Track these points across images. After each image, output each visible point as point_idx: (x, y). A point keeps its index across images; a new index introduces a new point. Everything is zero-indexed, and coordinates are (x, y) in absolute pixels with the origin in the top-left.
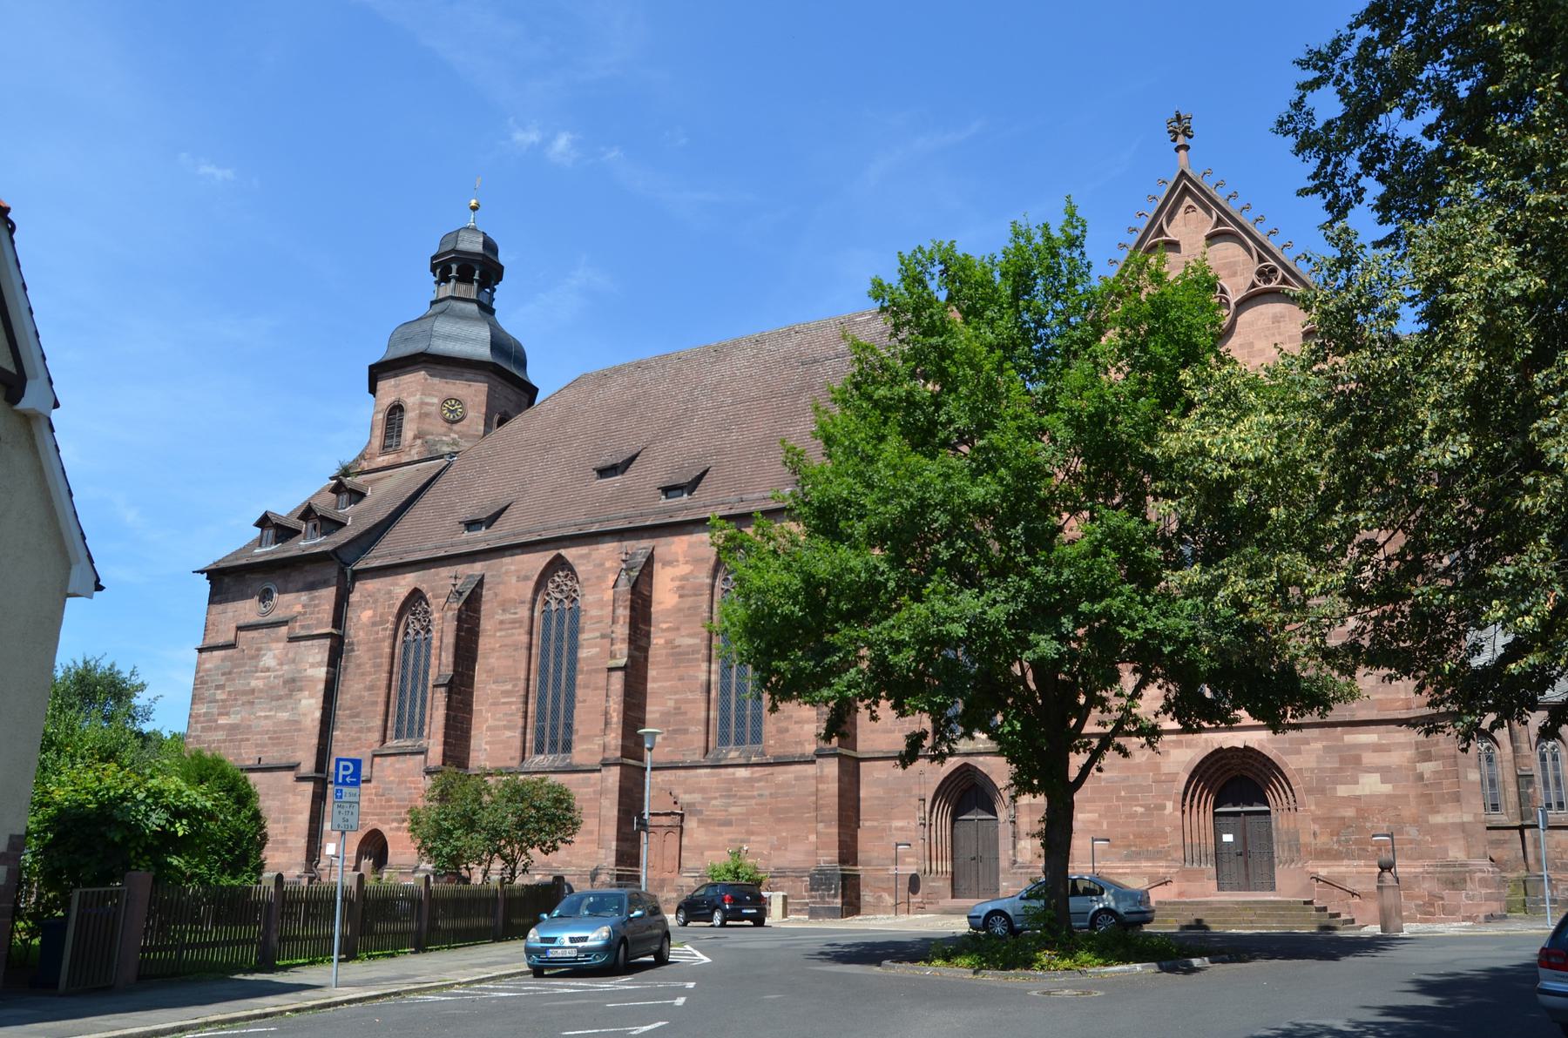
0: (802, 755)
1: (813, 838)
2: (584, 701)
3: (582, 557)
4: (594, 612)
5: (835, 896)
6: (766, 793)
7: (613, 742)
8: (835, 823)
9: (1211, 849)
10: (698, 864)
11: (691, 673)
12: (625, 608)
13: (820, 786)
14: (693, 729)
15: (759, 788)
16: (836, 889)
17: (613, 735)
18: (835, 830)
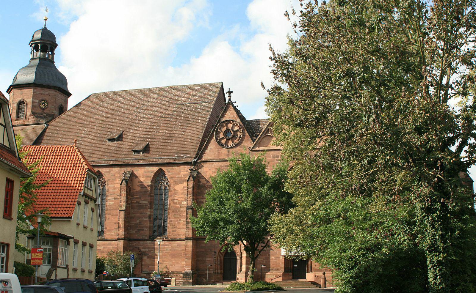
0: (180, 239)
1: (183, 263)
2: (109, 219)
3: (107, 172)
4: (112, 191)
5: (190, 279)
6: (169, 249)
7: (121, 233)
8: (191, 259)
9: (291, 268)
10: (147, 270)
11: (145, 212)
12: (125, 191)
13: (186, 248)
14: (145, 229)
15: (167, 248)
16: (191, 277)
17: (121, 231)
18: (191, 261)
